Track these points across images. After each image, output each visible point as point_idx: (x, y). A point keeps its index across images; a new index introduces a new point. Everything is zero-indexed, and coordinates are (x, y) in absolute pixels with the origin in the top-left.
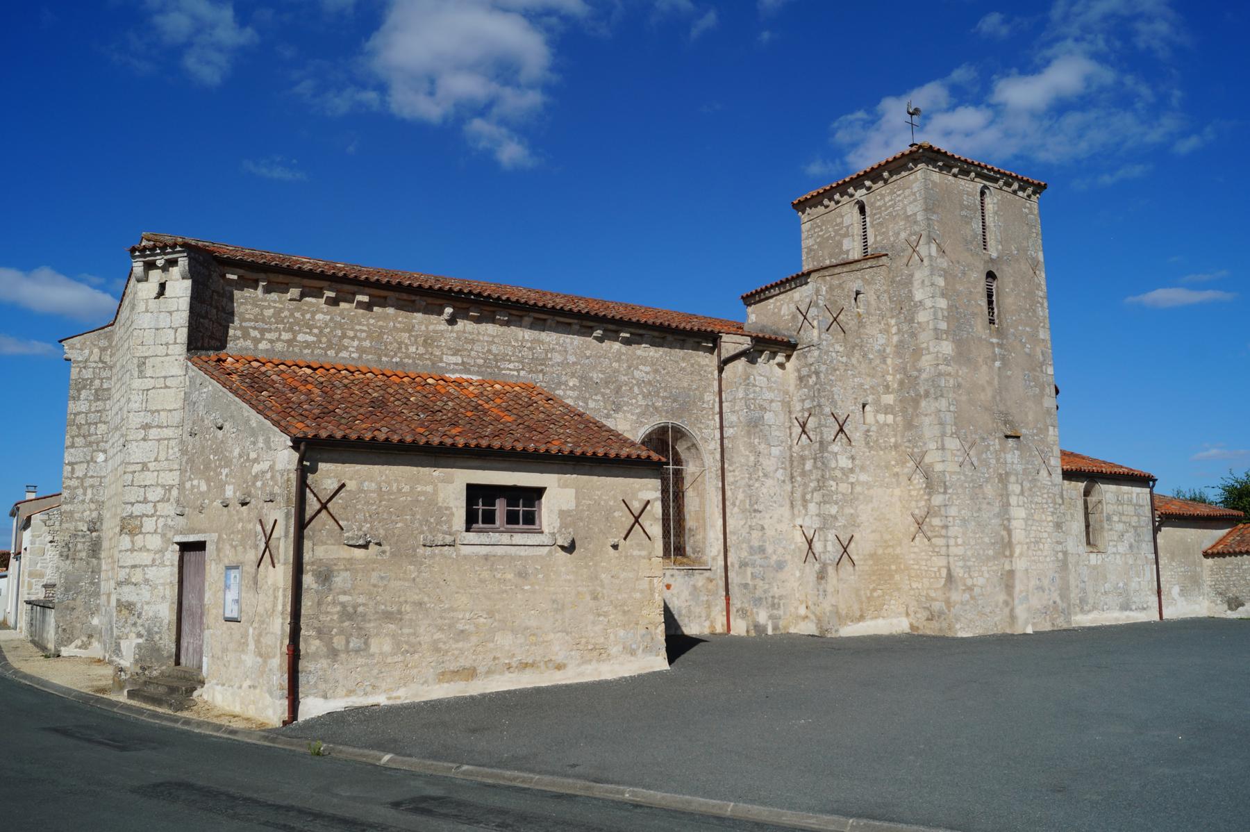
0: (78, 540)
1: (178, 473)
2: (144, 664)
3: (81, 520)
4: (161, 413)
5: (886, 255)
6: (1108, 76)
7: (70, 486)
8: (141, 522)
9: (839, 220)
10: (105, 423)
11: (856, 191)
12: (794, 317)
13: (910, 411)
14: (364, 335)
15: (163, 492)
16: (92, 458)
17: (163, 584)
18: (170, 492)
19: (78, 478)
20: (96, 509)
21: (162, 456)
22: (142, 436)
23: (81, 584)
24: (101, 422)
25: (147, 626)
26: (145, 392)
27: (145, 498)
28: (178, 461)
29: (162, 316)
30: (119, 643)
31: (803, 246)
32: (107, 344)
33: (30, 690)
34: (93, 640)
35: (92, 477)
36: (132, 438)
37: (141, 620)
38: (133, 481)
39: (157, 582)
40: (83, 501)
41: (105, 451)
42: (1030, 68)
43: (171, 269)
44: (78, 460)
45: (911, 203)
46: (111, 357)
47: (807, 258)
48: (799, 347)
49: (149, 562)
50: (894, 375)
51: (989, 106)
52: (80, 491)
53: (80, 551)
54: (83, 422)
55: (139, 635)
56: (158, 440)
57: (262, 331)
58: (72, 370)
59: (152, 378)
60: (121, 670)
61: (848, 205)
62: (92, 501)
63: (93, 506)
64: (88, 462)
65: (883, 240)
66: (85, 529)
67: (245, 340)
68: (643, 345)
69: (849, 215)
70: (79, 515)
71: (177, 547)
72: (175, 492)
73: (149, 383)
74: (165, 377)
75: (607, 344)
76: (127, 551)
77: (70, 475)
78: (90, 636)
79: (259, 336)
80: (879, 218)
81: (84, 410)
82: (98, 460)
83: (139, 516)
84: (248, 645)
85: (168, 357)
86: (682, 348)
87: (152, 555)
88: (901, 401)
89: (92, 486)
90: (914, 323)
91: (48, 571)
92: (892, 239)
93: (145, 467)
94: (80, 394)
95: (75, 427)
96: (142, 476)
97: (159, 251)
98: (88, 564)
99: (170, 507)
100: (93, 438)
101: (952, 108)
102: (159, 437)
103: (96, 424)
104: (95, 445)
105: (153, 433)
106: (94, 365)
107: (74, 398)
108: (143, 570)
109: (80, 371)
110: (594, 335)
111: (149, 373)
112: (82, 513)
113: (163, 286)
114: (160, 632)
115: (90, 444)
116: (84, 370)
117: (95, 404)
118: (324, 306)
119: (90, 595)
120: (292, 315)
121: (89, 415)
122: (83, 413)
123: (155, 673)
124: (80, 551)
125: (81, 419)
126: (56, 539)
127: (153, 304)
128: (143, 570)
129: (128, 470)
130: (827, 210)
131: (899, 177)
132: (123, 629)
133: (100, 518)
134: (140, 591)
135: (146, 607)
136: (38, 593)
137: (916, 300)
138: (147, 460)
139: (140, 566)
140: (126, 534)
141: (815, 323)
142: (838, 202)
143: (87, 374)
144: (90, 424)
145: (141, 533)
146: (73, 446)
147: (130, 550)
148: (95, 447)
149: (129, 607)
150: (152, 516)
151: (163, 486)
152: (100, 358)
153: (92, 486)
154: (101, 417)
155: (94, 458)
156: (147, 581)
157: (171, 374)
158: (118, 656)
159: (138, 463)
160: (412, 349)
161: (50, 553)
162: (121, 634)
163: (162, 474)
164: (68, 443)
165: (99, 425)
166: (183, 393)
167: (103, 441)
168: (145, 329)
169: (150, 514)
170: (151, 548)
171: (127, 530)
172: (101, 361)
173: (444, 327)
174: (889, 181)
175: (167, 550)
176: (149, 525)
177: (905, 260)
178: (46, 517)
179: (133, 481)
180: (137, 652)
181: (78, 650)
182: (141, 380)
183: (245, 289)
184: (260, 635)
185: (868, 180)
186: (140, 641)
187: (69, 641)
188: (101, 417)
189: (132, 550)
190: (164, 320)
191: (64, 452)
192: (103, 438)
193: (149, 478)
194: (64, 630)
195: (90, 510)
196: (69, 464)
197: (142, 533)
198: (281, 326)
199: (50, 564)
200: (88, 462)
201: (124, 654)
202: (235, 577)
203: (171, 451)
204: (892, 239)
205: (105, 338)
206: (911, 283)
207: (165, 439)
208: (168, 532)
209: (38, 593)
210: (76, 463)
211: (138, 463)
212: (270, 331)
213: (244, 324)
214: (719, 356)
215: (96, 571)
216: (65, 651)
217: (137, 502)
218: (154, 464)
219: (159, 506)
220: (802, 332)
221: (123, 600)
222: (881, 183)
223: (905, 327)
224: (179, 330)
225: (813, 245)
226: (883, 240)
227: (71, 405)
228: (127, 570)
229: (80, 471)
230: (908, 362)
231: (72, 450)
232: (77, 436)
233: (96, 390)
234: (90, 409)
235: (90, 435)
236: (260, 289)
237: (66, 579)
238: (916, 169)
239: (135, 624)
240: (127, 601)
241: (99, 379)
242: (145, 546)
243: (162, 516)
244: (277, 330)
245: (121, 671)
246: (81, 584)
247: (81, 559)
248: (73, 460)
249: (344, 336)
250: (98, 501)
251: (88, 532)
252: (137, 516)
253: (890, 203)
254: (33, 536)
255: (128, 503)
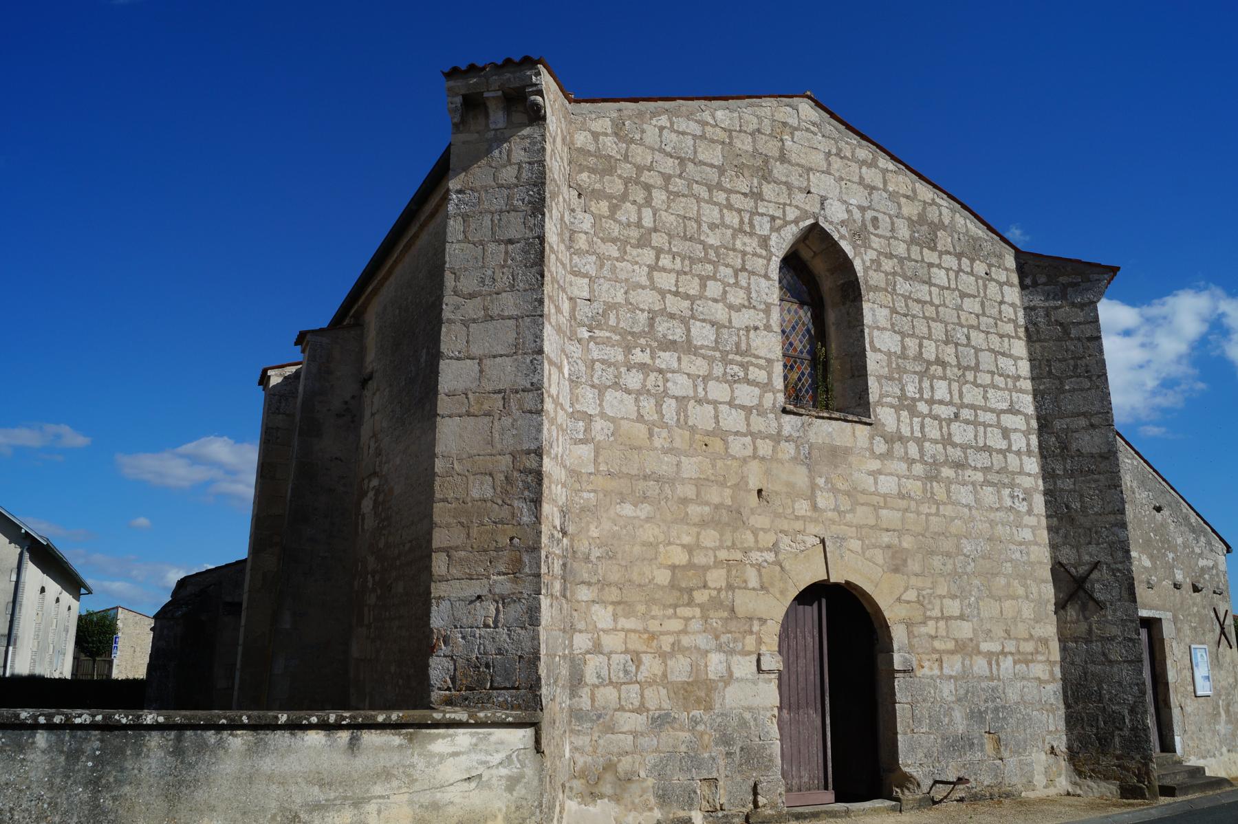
84: (1220, 716)
184: (1228, 705)
202: (1202, 655)
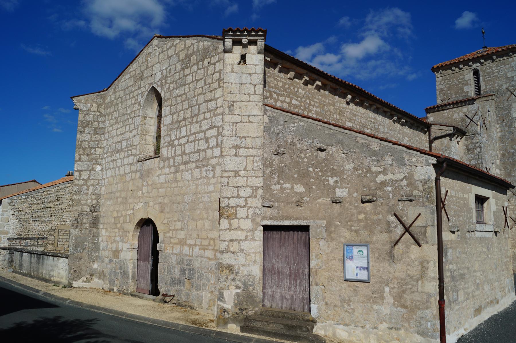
0: (84, 217)
1: (262, 179)
2: (241, 307)
3: (86, 205)
4: (247, 139)
5: (494, 95)
6: (388, 48)
7: (78, 184)
8: (236, 211)
9: (461, 77)
10: (101, 148)
11: (473, 64)
12: (463, 120)
13: (509, 168)
14: (317, 105)
15: (251, 191)
16: (93, 168)
17: (254, 253)
18: (257, 191)
19: (83, 179)
20: (95, 199)
21: (249, 167)
22: (234, 153)
23: (86, 243)
24: (98, 147)
25: (243, 281)
26: (235, 124)
27: (238, 195)
28: (261, 171)
29: (244, 76)
30: (223, 293)
31: (437, 88)
32: (102, 101)
33: (126, 321)
34: (94, 277)
35: (93, 179)
36: (226, 154)
37: (239, 277)
38: (228, 183)
39: (250, 251)
40: (87, 194)
41: (101, 165)
42: (357, 40)
43: (249, 46)
44: (84, 169)
45: (510, 71)
46: (104, 109)
47: (440, 94)
48: (467, 134)
49: (243, 238)
50: (499, 151)
51: (340, 54)
52: (85, 188)
53: (85, 224)
54: (87, 146)
55: (238, 287)
56: (246, 157)
57: (278, 95)
58: (79, 115)
59: (240, 115)
60: (225, 311)
61: (468, 70)
62: (93, 194)
63: (93, 197)
64: (90, 171)
65: (491, 88)
66: (88, 210)
67: (271, 99)
68: (407, 127)
69: (468, 75)
70: (84, 202)
71: (262, 228)
72: (260, 192)
73: (238, 119)
74: (249, 116)
75: (396, 124)
76: (226, 230)
77: (78, 178)
78: (92, 275)
79: (277, 98)
80: (489, 78)
81: (87, 139)
82: (97, 170)
83: (235, 207)
85: (250, 103)
86: (417, 130)
87: (245, 233)
88: (503, 163)
89: (93, 185)
90: (512, 127)
91: (11, 231)
92: (497, 88)
93: (237, 174)
94: (84, 130)
95: (81, 149)
96: (235, 180)
97: (246, 33)
98: (90, 231)
99: (257, 202)
100: (93, 156)
101: (325, 54)
102: (246, 155)
103: (95, 148)
104: (94, 161)
105: (242, 152)
106: (94, 113)
107: (81, 132)
108: (239, 243)
109: (85, 116)
110: (394, 119)
111: (237, 112)
112: (86, 201)
113: (243, 57)
114: (253, 285)
115: (91, 160)
116: (87, 116)
117: (94, 136)
118: (302, 85)
119: (92, 250)
120: (289, 87)
121: (90, 143)
122: (86, 141)
123: (250, 313)
124: (85, 224)
125: (85, 145)
126: (15, 213)
127: (236, 68)
128: (239, 243)
129: (224, 175)
130: (453, 72)
131: (502, 59)
132: (225, 283)
133: (98, 204)
134: (236, 257)
135: (242, 268)
136: (5, 243)
137: (513, 116)
138: (238, 170)
139: (236, 240)
140: (225, 218)
141: (479, 123)
142: (460, 69)
143: (89, 118)
144: (91, 148)
145: (236, 218)
146: (80, 160)
147: (228, 229)
148: (94, 162)
149: (229, 268)
150: (244, 207)
151: (251, 187)
152: (97, 109)
153: (93, 185)
154: (98, 144)
155: (94, 169)
156: (242, 251)
157: (253, 114)
158: (221, 301)
159: (231, 171)
160: (335, 116)
161: (12, 221)
162: (223, 286)
163: (250, 179)
164: (77, 158)
165: (97, 149)
166: (262, 127)
167: (100, 159)
168: (232, 83)
169: (242, 205)
170: (244, 228)
171: (226, 216)
172: (98, 111)
173: (345, 105)
174: (495, 61)
175: (256, 230)
176: (242, 212)
177: (506, 98)
178: (10, 201)
179: (228, 183)
180: (236, 298)
181: (84, 283)
182: (231, 116)
183: (270, 68)
185: (482, 59)
186: (238, 291)
187: (78, 278)
188: (98, 144)
189: (230, 229)
190: (246, 79)
191: (74, 164)
192: (100, 156)
193: (241, 181)
194: (75, 271)
195: (92, 199)
196: (77, 171)
197: (238, 218)
198: (285, 93)
199: (12, 227)
200: (90, 171)
201: (226, 300)
203: (255, 164)
204: (497, 88)
205: (101, 98)
206: (511, 109)
207: (251, 156)
208: (257, 218)
209: (5, 243)
210: (82, 171)
211: (231, 171)
212: (281, 95)
213: (270, 89)
214: (430, 135)
215: (96, 236)
216: (75, 284)
217: (233, 197)
218: (243, 172)
219: (249, 200)
220: (469, 127)
221: (224, 263)
222: (489, 61)
223: (506, 129)
224: (257, 86)
225: (444, 88)
226: (491, 88)
227: (79, 136)
228: (227, 243)
229: (85, 175)
230: (508, 145)
231: (80, 163)
232: (83, 155)
233: (95, 128)
234: (91, 139)
235: (91, 154)
236: (277, 69)
237: (76, 240)
238: (513, 56)
239: (234, 280)
240: (227, 264)
241: (97, 121)
242: (239, 227)
243: (252, 207)
244: (284, 95)
245: (224, 312)
246: (86, 243)
247: (86, 228)
248: (80, 169)
249: (310, 104)
250: (96, 194)
251: (90, 213)
252: (233, 207)
253: (496, 71)
254: (3, 211)
255: (225, 198)
